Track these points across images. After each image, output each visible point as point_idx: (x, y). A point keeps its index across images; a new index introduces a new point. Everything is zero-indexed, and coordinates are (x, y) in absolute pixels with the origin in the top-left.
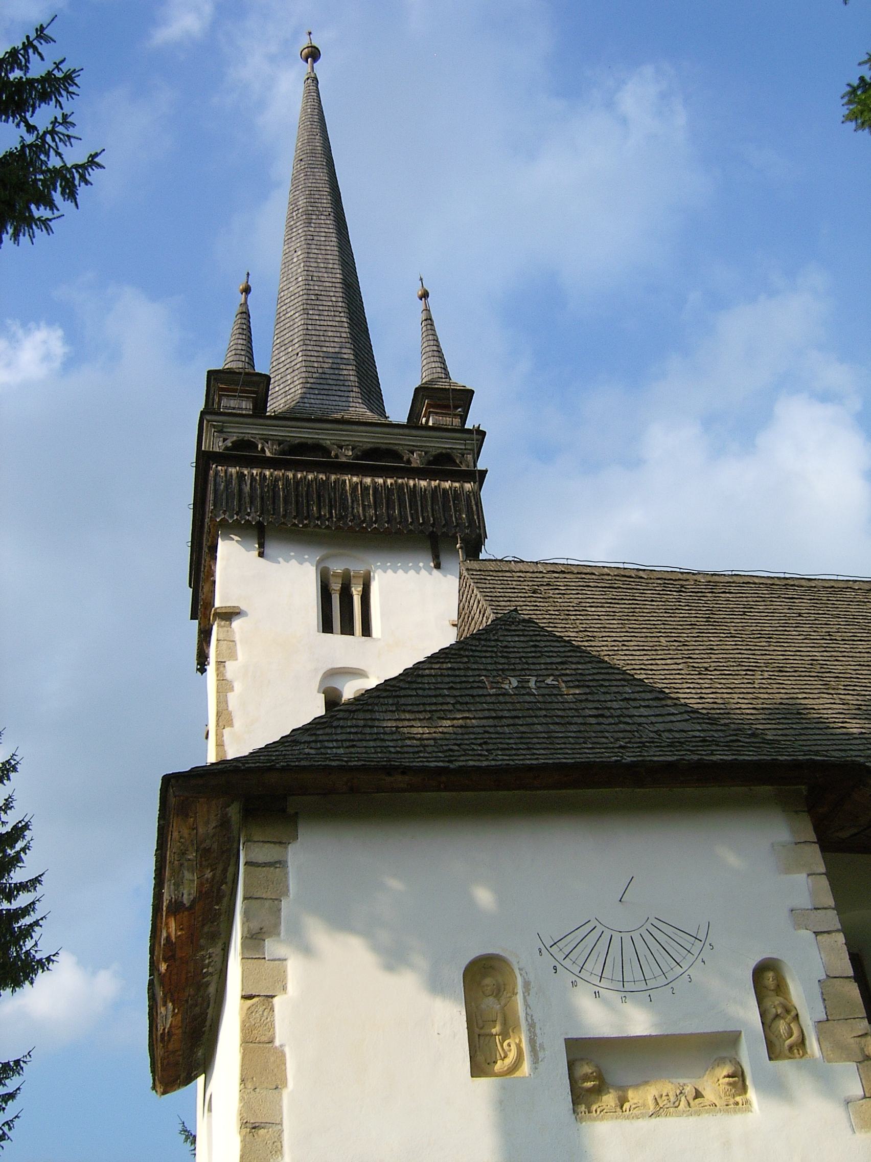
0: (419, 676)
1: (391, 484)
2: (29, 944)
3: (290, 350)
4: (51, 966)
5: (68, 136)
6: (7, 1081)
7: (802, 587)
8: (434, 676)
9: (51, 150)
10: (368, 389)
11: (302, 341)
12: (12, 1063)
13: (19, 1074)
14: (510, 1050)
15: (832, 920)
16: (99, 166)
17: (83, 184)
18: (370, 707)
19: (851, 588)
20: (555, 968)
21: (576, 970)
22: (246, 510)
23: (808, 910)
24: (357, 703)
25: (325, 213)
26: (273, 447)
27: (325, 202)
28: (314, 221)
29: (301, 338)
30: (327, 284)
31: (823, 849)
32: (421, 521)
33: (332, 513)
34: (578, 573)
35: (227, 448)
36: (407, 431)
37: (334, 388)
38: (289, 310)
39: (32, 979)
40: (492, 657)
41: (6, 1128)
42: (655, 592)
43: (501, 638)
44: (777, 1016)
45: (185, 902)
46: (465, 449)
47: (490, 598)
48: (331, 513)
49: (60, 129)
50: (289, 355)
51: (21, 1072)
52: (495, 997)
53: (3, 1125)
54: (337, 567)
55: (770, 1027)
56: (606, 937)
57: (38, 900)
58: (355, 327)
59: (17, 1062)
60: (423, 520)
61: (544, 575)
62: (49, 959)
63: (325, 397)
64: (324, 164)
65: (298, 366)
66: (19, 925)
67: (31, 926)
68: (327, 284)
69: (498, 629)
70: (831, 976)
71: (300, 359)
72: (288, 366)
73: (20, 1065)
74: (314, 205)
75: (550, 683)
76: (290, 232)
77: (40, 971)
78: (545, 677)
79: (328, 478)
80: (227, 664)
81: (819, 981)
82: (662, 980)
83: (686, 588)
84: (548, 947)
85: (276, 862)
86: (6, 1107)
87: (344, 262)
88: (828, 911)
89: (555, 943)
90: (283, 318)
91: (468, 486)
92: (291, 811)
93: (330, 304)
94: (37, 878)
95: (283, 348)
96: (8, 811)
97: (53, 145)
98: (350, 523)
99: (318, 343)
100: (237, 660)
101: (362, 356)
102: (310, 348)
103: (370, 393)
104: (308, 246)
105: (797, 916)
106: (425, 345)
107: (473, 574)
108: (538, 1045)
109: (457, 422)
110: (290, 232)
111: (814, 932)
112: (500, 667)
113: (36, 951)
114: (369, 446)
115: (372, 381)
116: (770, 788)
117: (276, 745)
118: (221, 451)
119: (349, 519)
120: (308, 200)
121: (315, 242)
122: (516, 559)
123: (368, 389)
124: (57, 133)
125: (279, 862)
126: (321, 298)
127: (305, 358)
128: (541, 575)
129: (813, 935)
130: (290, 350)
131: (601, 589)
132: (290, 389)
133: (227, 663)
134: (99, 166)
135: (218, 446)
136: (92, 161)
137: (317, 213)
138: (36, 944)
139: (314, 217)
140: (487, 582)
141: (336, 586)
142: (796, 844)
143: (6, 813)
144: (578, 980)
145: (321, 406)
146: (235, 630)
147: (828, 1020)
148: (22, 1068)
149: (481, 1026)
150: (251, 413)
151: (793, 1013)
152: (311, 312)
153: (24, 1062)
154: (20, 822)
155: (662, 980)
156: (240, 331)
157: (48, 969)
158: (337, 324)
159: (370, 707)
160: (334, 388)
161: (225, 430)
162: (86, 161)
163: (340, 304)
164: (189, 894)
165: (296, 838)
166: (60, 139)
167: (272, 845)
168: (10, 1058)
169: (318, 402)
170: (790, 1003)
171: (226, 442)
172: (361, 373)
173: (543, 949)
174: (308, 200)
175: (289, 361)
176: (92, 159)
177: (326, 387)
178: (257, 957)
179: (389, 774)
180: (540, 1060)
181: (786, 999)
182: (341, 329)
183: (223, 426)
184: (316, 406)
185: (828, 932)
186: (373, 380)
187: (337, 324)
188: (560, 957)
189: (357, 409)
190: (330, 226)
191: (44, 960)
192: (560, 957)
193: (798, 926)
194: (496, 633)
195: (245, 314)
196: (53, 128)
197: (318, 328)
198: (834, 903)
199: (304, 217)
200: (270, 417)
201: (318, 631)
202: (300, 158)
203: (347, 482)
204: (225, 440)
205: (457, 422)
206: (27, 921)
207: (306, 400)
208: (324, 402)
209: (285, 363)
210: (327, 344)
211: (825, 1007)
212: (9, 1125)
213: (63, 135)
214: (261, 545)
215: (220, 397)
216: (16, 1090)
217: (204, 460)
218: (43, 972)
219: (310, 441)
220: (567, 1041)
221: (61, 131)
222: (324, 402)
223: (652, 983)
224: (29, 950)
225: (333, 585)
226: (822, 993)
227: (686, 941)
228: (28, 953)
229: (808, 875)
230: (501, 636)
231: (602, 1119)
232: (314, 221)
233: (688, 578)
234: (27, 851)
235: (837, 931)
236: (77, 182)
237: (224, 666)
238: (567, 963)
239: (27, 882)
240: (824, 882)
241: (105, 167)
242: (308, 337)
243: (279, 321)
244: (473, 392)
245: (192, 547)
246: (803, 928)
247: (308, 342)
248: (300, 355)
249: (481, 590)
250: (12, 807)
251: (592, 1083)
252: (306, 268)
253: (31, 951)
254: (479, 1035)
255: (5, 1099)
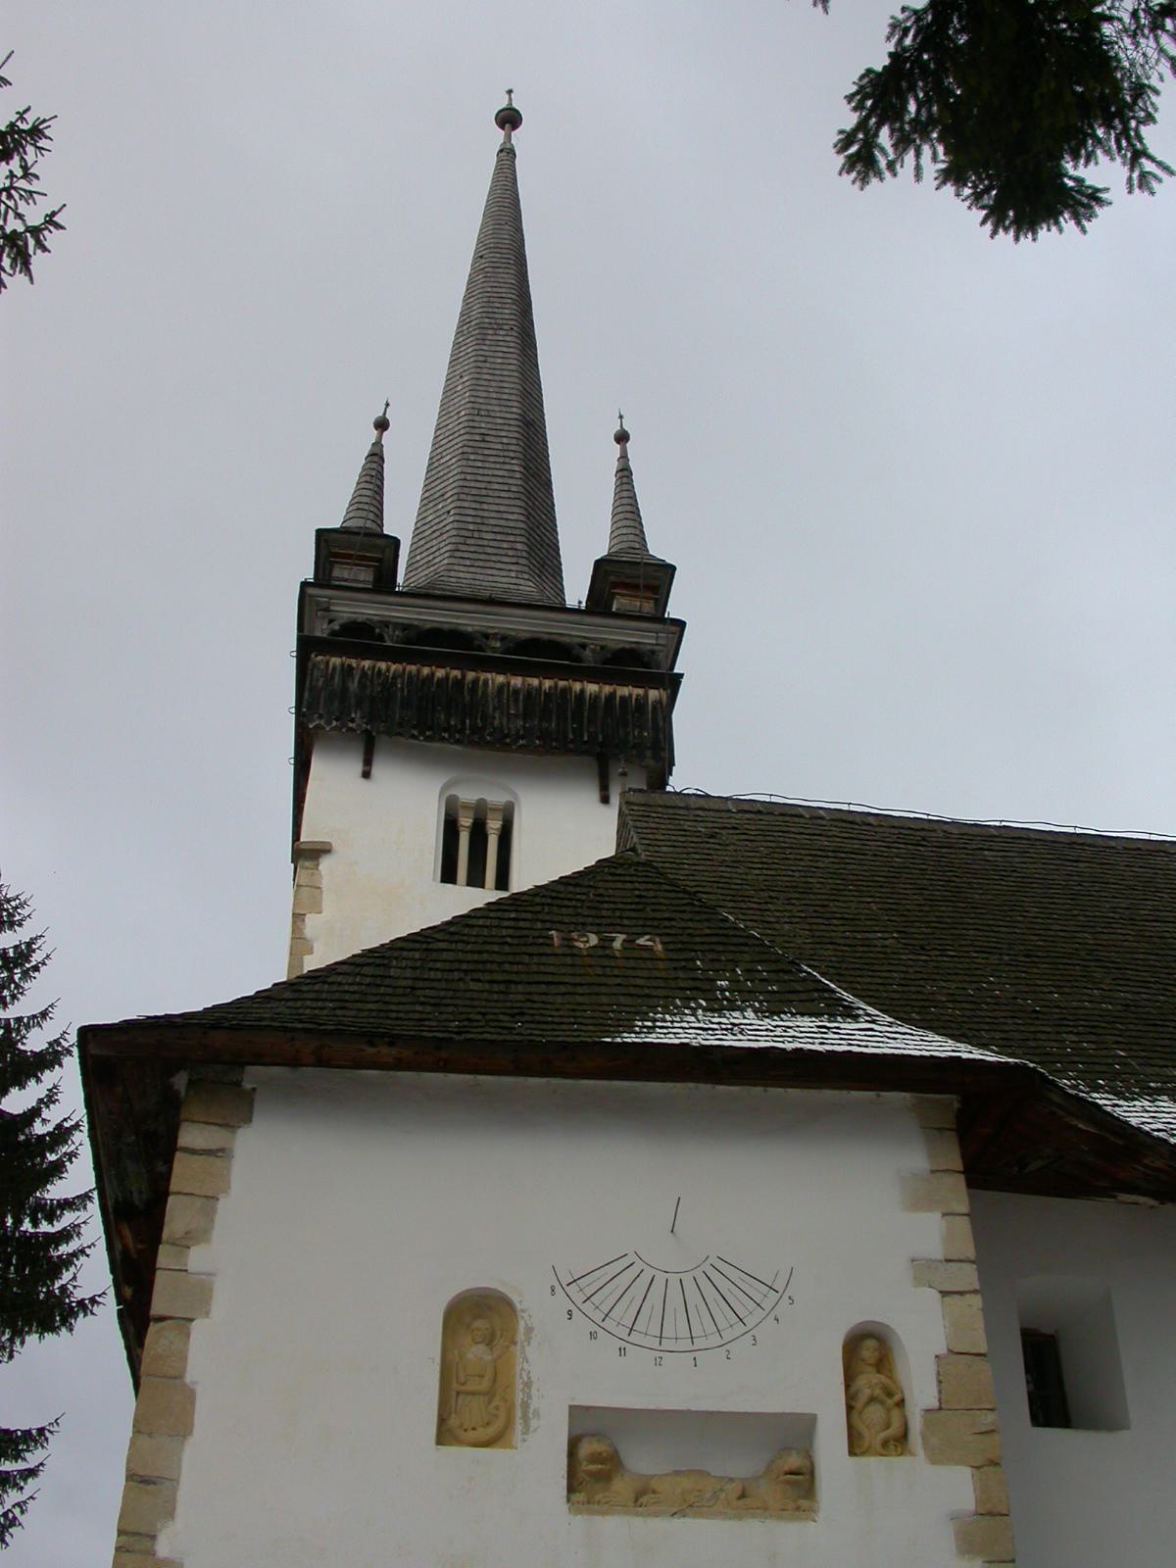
0: (467, 926)
1: (550, 688)
2: (66, 1276)
3: (440, 506)
4: (95, 1309)
5: (31, 193)
6: (28, 1455)
7: (1095, 847)
8: (487, 927)
9: (10, 211)
10: (541, 562)
11: (456, 496)
12: (34, 1432)
13: (43, 1447)
14: (496, 1416)
15: (968, 1276)
16: (59, 226)
17: (39, 251)
18: (385, 962)
19: (1164, 852)
20: (570, 1313)
21: (598, 1317)
22: (350, 714)
23: (935, 1261)
24: (370, 955)
25: (505, 327)
26: (394, 632)
27: (508, 312)
28: (490, 337)
29: (455, 491)
30: (499, 421)
31: (971, 1184)
32: (586, 738)
33: (465, 723)
34: (781, 815)
35: (333, 633)
36: (588, 619)
37: (494, 558)
38: (444, 453)
39: (71, 1324)
40: (575, 907)
41: (17, 1511)
42: (883, 844)
43: (600, 884)
44: (872, 1399)
45: (137, 1202)
46: (657, 645)
47: (647, 842)
48: (464, 723)
49: (22, 184)
50: (438, 514)
51: (45, 1445)
52: (487, 1345)
53: (14, 1506)
54: (468, 795)
55: (861, 1412)
56: (689, 1286)
57: (84, 1223)
58: (531, 478)
59: (41, 1431)
60: (588, 737)
61: (733, 815)
62: (93, 1300)
63: (479, 570)
64: (512, 262)
65: (447, 528)
66: (59, 1253)
67: (74, 1255)
68: (499, 421)
69: (598, 873)
70: (955, 1351)
71: (452, 519)
72: (435, 528)
73: (44, 1435)
74: (491, 315)
75: (642, 943)
76: (457, 352)
77: (81, 1315)
78: (635, 936)
79: (464, 677)
80: (307, 918)
81: (937, 1356)
82: (715, 1340)
83: (928, 842)
84: (563, 1286)
85: (219, 1150)
86: (25, 1487)
87: (526, 393)
88: (964, 1264)
89: (575, 1281)
90: (436, 464)
91: (653, 694)
92: (247, 1086)
93: (500, 447)
94: (86, 1193)
95: (431, 504)
96: (51, 1106)
97: (11, 203)
98: (488, 738)
99: (477, 498)
100: (320, 912)
101: (537, 517)
102: (466, 504)
103: (543, 567)
104: (478, 370)
105: (922, 1270)
106: (618, 503)
107: (633, 810)
108: (531, 1411)
109: (648, 607)
110: (457, 352)
111: (941, 1292)
112: (581, 920)
113: (75, 1287)
114: (529, 635)
115: (548, 551)
116: (908, 1095)
117: (245, 1000)
118: (324, 635)
119: (488, 731)
120: (484, 310)
121: (488, 365)
122: (699, 793)
123: (541, 562)
124: (16, 189)
125: (222, 1150)
126: (487, 438)
127: (458, 518)
128: (729, 815)
129: (939, 1296)
130: (440, 506)
131: (807, 837)
132: (434, 558)
133: (307, 916)
134: (59, 226)
135: (321, 630)
136: (50, 220)
137: (495, 327)
138: (74, 1278)
139: (490, 332)
140: (651, 820)
141: (466, 821)
142: (933, 1172)
143: (48, 1107)
144: (601, 1332)
145: (473, 582)
146: (323, 873)
147: (940, 1409)
148: (47, 1439)
149: (462, 1380)
150: (370, 587)
151: (897, 1398)
152: (472, 457)
153: (51, 1432)
154: (65, 1120)
155: (715, 1340)
156: (368, 478)
157: (92, 1313)
158: (505, 473)
159: (385, 962)
160: (494, 558)
161: (332, 608)
162: (43, 221)
163: (513, 448)
164: (140, 1193)
165: (248, 1120)
166: (21, 195)
167: (216, 1128)
168: (17, 1423)
169: (468, 576)
170: (895, 1383)
171: (332, 624)
172: (532, 540)
173: (558, 1289)
174: (484, 310)
175: (437, 520)
176: (51, 219)
177: (482, 557)
178: (177, 1268)
179: (372, 1044)
180: (531, 1429)
181: (891, 1378)
182: (510, 481)
183: (329, 603)
184: (464, 581)
185: (961, 1293)
186: (551, 551)
187: (505, 473)
188: (579, 1298)
189: (521, 587)
190: (512, 345)
191: (87, 1302)
192: (579, 1298)
193: (919, 1280)
194: (594, 877)
195: (376, 456)
196: (11, 183)
197: (480, 478)
198: (182, 1072)
199: (477, 332)
200: (400, 594)
201: (434, 880)
202: (480, 254)
203: (490, 682)
204: (331, 621)
205: (648, 607)
206: (65, 1249)
207: (452, 574)
208: (477, 577)
209: (432, 523)
210: (490, 500)
211: (940, 1392)
212: (21, 1508)
213: (25, 191)
214: (368, 762)
215: (332, 564)
216: (38, 1466)
217: (307, 646)
218: (85, 1316)
219: (446, 627)
220: (572, 1408)
221: (21, 186)
222: (477, 577)
223: (699, 1343)
224: (66, 1285)
225: (461, 819)
226: (938, 1373)
227: (757, 1291)
228: (63, 1288)
229: (944, 1215)
230: (600, 881)
231: (604, 1513)
232: (490, 337)
233: (936, 828)
234: (73, 1159)
235: (975, 1292)
236: (31, 252)
237: (303, 920)
238: (587, 1307)
239: (73, 1199)
240: (964, 1226)
241: (66, 226)
242: (466, 490)
243: (432, 467)
244: (674, 568)
245: (295, 765)
246: (924, 1285)
247: (462, 497)
248: (451, 513)
249: (640, 831)
250: (57, 1100)
251: (600, 1466)
252: (472, 399)
253: (68, 1286)
254: (458, 1393)
255: (24, 1476)
